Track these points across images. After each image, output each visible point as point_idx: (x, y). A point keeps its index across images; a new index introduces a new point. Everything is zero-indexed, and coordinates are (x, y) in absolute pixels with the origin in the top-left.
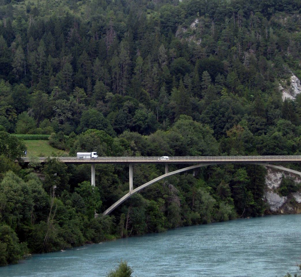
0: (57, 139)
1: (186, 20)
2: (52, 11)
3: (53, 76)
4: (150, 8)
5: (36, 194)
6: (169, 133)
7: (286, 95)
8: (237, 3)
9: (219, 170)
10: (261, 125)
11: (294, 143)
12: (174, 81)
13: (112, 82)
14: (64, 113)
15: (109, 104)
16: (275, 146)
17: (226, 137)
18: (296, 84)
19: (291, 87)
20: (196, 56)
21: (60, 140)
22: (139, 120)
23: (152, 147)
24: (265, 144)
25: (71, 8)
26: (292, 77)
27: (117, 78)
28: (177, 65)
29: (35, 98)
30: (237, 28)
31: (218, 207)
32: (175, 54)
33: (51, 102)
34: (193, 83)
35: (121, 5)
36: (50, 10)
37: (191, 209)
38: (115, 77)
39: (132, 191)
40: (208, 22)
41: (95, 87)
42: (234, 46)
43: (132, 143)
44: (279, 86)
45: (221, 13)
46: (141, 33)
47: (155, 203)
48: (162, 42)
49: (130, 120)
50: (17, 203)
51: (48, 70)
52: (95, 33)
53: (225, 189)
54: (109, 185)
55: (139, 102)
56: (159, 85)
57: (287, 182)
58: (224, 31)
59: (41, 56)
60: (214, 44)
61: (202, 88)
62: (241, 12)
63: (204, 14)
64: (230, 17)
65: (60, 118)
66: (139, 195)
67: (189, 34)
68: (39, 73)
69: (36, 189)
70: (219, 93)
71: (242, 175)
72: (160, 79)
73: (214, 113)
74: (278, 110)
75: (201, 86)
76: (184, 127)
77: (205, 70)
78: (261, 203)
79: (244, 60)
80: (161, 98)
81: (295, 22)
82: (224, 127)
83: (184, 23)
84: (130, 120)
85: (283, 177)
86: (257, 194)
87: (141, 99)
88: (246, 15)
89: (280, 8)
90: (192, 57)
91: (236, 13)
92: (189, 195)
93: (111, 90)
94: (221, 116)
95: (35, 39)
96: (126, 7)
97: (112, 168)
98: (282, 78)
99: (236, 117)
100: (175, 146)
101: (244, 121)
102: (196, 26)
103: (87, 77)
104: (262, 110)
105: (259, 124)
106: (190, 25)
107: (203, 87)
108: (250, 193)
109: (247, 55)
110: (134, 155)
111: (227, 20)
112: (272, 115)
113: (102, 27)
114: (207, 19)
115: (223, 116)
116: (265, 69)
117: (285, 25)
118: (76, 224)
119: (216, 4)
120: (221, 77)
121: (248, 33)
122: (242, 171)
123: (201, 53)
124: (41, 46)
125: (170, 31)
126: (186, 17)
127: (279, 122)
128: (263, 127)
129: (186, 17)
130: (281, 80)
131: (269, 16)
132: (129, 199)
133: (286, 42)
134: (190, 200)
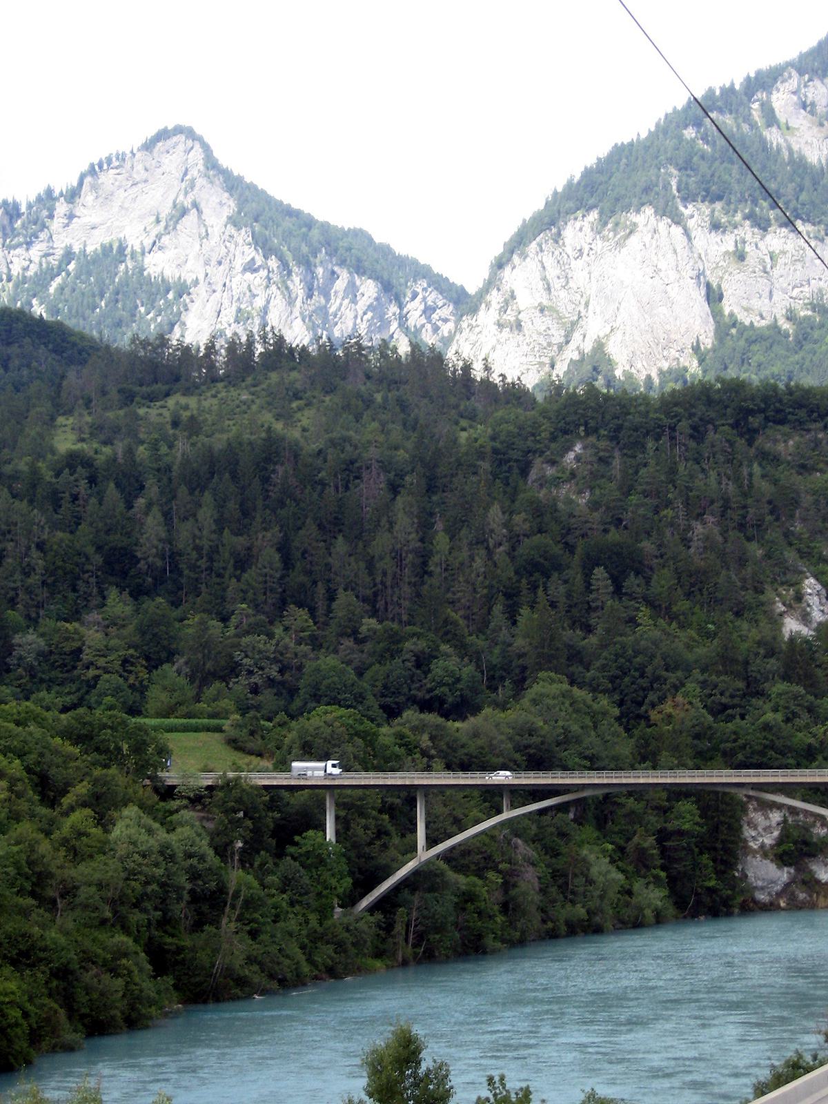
0: (245, 730)
1: (553, 445)
2: (231, 423)
3: (234, 580)
5: (194, 861)
7: (791, 626)
8: (676, 405)
11: (811, 740)
13: (375, 594)
14: (262, 669)
15: (368, 646)
17: (650, 726)
18: (816, 598)
19: (804, 605)
20: (578, 533)
21: (252, 733)
22: (441, 684)
23: (472, 748)
24: (741, 742)
25: (278, 417)
26: (807, 582)
29: (190, 631)
30: (675, 463)
31: (629, 893)
32: (527, 526)
34: (569, 595)
35: (398, 409)
36: (227, 422)
38: (382, 583)
39: (424, 854)
42: (667, 507)
43: (425, 740)
45: (636, 430)
46: (445, 476)
47: (480, 882)
48: (495, 498)
50: (147, 883)
51: (222, 564)
52: (335, 475)
53: (646, 849)
55: (439, 641)
56: (489, 601)
58: (643, 471)
61: (590, 607)
62: (684, 426)
64: (657, 439)
65: (252, 680)
66: (443, 865)
67: (559, 478)
70: (632, 621)
71: (687, 816)
73: (620, 668)
74: (772, 661)
75: (588, 603)
76: (548, 700)
77: (598, 565)
78: (733, 884)
79: (691, 540)
80: (494, 631)
83: (548, 453)
85: (785, 821)
86: (723, 862)
87: (446, 633)
88: (697, 433)
89: (779, 416)
90: (568, 534)
91: (673, 429)
92: (560, 863)
93: (374, 613)
94: (637, 674)
95: (192, 491)
96: (409, 415)
98: (782, 584)
99: (673, 677)
101: (690, 686)
102: (578, 458)
103: (315, 583)
104: (734, 661)
105: (727, 694)
106: (563, 456)
107: (593, 605)
108: (705, 859)
109: (699, 528)
110: (428, 768)
111: (651, 444)
113: (352, 462)
114: (603, 444)
115: (642, 676)
116: (742, 561)
118: (291, 934)
120: (637, 582)
121: (701, 476)
123: (589, 525)
124: (205, 509)
125: (516, 471)
126: (553, 438)
128: (736, 701)
129: (553, 438)
130: (780, 589)
131: (751, 435)
132: (416, 873)
133: (793, 498)
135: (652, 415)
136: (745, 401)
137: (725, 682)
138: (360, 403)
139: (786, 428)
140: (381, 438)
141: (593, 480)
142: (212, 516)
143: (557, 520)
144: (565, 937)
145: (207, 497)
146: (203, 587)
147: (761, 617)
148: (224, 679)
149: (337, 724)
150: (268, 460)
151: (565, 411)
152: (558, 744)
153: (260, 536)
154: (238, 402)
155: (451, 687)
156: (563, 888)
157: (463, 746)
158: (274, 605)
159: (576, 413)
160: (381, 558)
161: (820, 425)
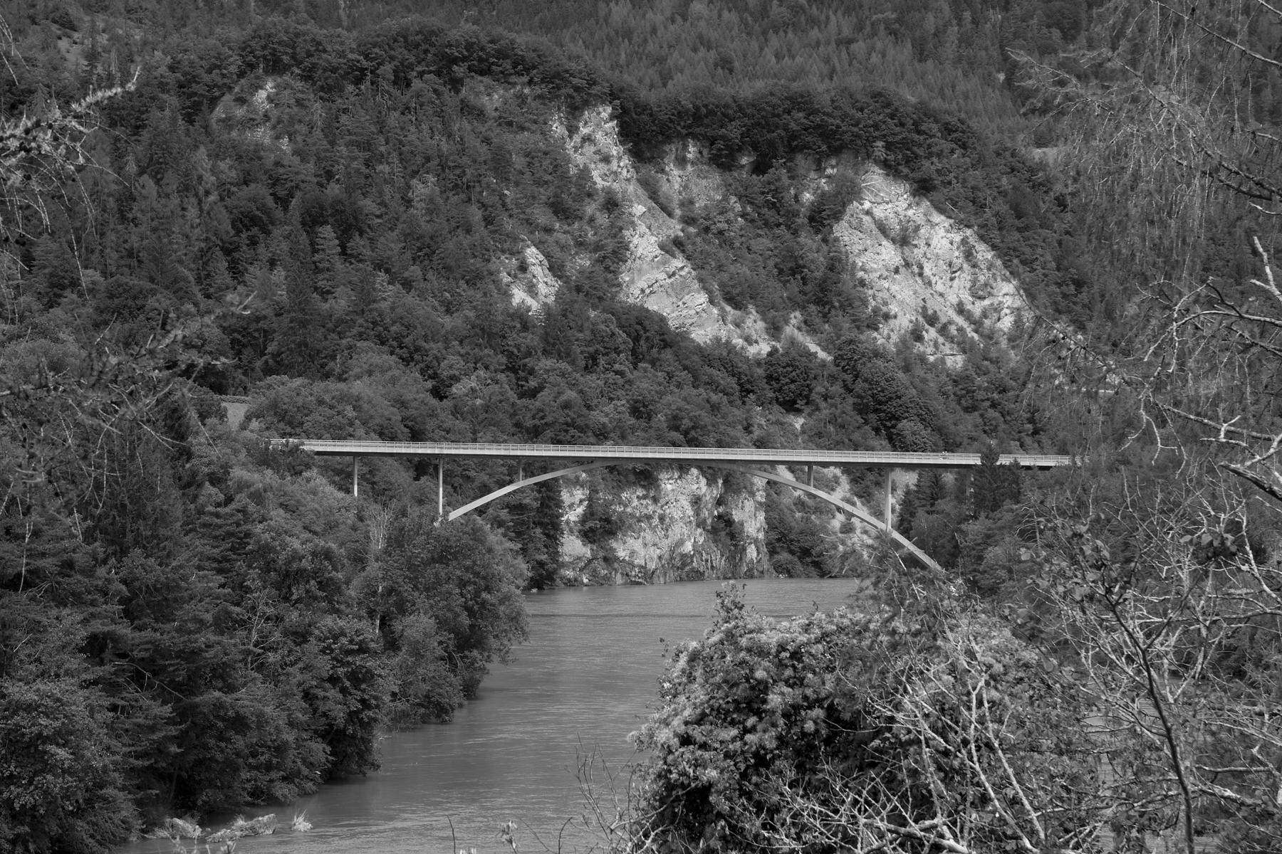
16: (567, 424)
20: (289, 185)
45: (334, 70)
62: (387, 69)
67: (253, 120)
72: (207, 239)
88: (402, 81)
89: (484, 66)
98: (503, 252)
102: (270, 99)
107: (321, 266)
114: (299, 85)
129: (241, 74)
131: (456, 84)
139: (487, 80)
141: (283, 127)
161: (525, 79)
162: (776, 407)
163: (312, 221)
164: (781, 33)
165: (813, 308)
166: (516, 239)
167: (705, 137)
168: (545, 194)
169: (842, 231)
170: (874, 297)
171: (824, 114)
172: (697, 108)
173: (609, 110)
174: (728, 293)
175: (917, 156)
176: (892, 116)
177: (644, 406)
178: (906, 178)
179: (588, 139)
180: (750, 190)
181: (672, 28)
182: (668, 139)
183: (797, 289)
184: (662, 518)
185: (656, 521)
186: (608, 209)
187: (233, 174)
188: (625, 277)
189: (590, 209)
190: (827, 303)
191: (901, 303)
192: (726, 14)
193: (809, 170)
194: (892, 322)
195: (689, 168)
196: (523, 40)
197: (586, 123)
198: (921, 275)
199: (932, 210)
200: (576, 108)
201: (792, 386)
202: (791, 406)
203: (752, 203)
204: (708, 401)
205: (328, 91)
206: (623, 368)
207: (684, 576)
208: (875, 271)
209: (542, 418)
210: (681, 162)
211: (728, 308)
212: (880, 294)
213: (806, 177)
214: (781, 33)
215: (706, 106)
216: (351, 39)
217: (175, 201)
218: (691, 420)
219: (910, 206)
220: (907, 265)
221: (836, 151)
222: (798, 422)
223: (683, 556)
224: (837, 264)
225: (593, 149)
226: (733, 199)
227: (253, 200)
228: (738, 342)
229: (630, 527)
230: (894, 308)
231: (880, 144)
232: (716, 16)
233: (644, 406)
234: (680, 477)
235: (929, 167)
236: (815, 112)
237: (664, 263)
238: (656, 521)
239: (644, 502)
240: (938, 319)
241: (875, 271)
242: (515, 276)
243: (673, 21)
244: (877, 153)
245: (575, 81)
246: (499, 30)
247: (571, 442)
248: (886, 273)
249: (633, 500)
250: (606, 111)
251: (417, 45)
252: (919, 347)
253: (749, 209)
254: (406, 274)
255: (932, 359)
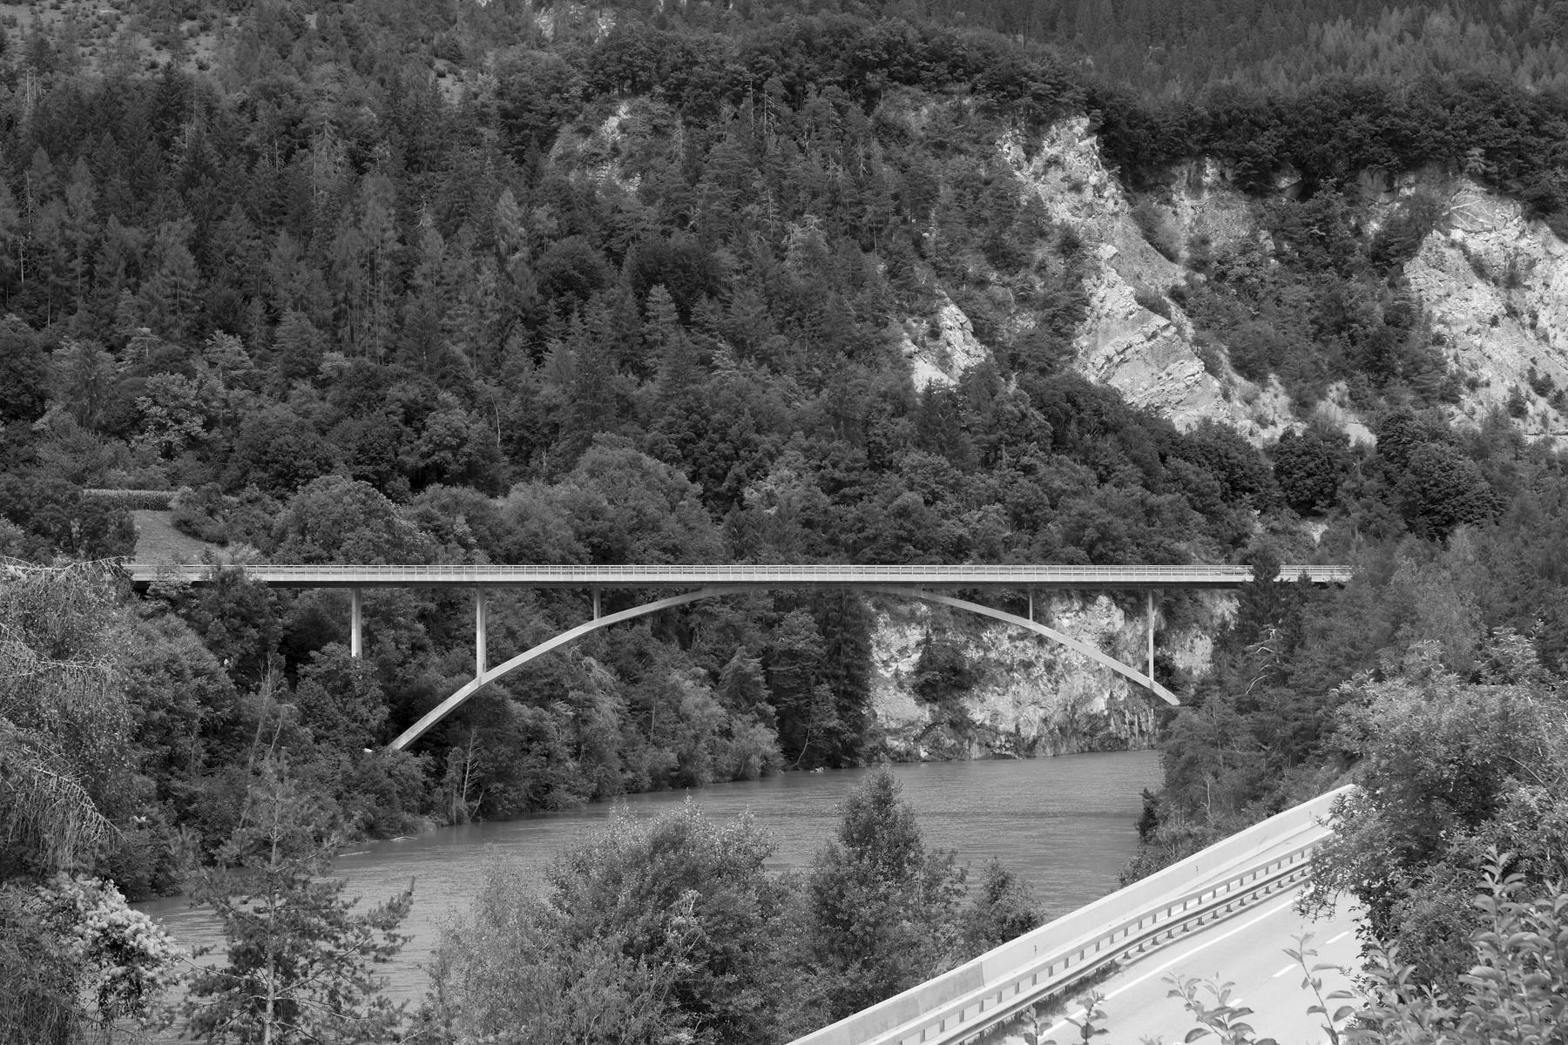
0: (200, 508)
1: (588, 107)
2: (87, 50)
3: (127, 292)
4: (443, 57)
5: (202, 681)
6: (561, 491)
7: (924, 373)
8: (764, 52)
9: (726, 613)
10: (849, 470)
11: (962, 531)
12: (553, 318)
13: (337, 317)
14: (179, 422)
15: (333, 393)
16: (900, 538)
17: (743, 509)
18: (959, 334)
19: (941, 343)
20: (626, 235)
21: (211, 513)
22: (440, 446)
23: (521, 534)
24: (870, 532)
25: (160, 45)
26: (946, 310)
27: (355, 302)
28: (563, 261)
29: (66, 364)
30: (762, 138)
31: (727, 734)
32: (553, 224)
33: (128, 380)
34: (616, 324)
35: (344, 41)
36: (81, 49)
37: (648, 738)
38: (346, 300)
39: (485, 676)
40: (663, 116)
41: (279, 331)
42: (750, 201)
43: (460, 525)
44: (901, 340)
45: (706, 87)
46: (432, 148)
47: (547, 715)
48: (506, 182)
49: (408, 448)
50: (153, 708)
51: (108, 268)
52: (270, 142)
53: (749, 675)
54: (401, 658)
55: (435, 387)
56: (501, 332)
57: (942, 658)
58: (716, 147)
59: (79, 220)
60: (683, 194)
61: (645, 341)
62: (775, 83)
63: (647, 87)
64: (736, 101)
65: (165, 438)
66: (501, 690)
67: (597, 155)
68: (76, 278)
69: (201, 665)
70: (706, 362)
71: (801, 631)
73: (694, 427)
74: (903, 421)
75: (642, 336)
76: (618, 470)
77: (657, 283)
78: (859, 725)
79: (786, 249)
80: (511, 373)
81: (956, 122)
82: (725, 474)
83: (581, 117)
84: (408, 448)
85: (928, 641)
86: (847, 694)
87: (443, 377)
88: (794, 96)
89: (911, 71)
90: (610, 236)
91: (758, 87)
92: (638, 692)
93: (336, 343)
94: (716, 437)
95: (54, 157)
96: (361, 51)
97: (413, 602)
98: (912, 313)
99: (767, 442)
100: (589, 535)
101: (790, 454)
102: (623, 128)
103: (247, 298)
104: (850, 421)
105: (842, 466)
106: (601, 124)
107: (650, 338)
108: (824, 689)
109: (797, 233)
110: (469, 561)
111: (727, 109)
112: (885, 434)
113: (295, 123)
114: (659, 107)
115: (723, 440)
116: (857, 281)
117: (922, 134)
118: (321, 779)
119: (689, 53)
120: (711, 307)
121: (800, 157)
122: (800, 619)
123: (641, 225)
124: (79, 184)
125: (534, 142)
126: (587, 97)
127: (907, 460)
128: (853, 476)
129: (587, 97)
130: (909, 320)
131: (870, 98)
132: (471, 701)
133: (928, 192)
134: (642, 709)
135: (729, 67)
136: (863, 48)
137: (839, 449)
138: (286, 28)
139: (916, 90)
140: (336, 88)
141: (637, 163)
142: (88, 196)
143: (597, 218)
144: (649, 791)
145: (81, 168)
146: (79, 302)
147: (883, 359)
148: (121, 435)
149: (347, 499)
150: (165, 114)
151: (604, 58)
152: (631, 531)
153: (164, 228)
154: (94, 18)
155: (455, 450)
156: (644, 726)
157: (509, 532)
158: (188, 329)
159: (620, 60)
160: (345, 266)
161: (966, 86)
162: (1287, 510)
163: (645, 280)
164: (1542, 46)
165: (1362, 376)
166: (931, 296)
167: (1228, 154)
168: (981, 234)
169: (1418, 274)
170: (1456, 359)
171: (1396, 115)
172: (1216, 115)
173: (1086, 122)
174: (1239, 358)
175: (1533, 167)
176: (1497, 114)
177: (1029, 511)
178: (1517, 196)
179: (1054, 162)
180: (1288, 222)
181: (1398, 48)
182: (1174, 158)
183: (1340, 351)
184: (1050, 667)
185: (1039, 670)
186: (1063, 251)
187: (553, 223)
188: (1083, 342)
189: (1041, 252)
190: (1382, 369)
191: (1499, 366)
192: (1472, 28)
193: (1377, 192)
194: (1482, 392)
195: (1206, 195)
196: (968, 35)
197: (1053, 141)
198: (1533, 326)
199: (1552, 237)
200: (1041, 122)
201: (1309, 482)
202: (1307, 509)
203: (1291, 239)
204: (1143, 503)
205: (702, 113)
206: (1033, 461)
207: (1095, 744)
208: (1462, 323)
209: (860, 530)
210: (1195, 188)
211: (1238, 379)
212: (1467, 354)
213: (1373, 202)
214: (1542, 46)
215: (1228, 112)
216: (732, 42)
217: (467, 262)
218: (1097, 529)
219: (1522, 233)
220: (1512, 313)
221: (1413, 164)
222: (1317, 531)
223: (1092, 718)
224: (1403, 317)
225: (1060, 174)
226: (1264, 234)
227: (569, 255)
228: (1244, 424)
229: (993, 679)
230: (1486, 373)
231: (1477, 151)
232: (1457, 31)
233: (1029, 511)
234: (1083, 609)
235: (1552, 179)
236: (1384, 113)
237: (1142, 321)
238: (1039, 670)
239: (1020, 644)
240: (1552, 385)
241: (1462, 323)
242: (923, 345)
243: (1401, 40)
244: (1472, 164)
245: (1034, 86)
246: (933, 24)
247: (907, 560)
248: (1476, 326)
249: (1004, 639)
250: (1081, 124)
251: (825, 49)
252: (1518, 424)
253: (1286, 246)
254: (764, 346)
255: (1531, 440)
